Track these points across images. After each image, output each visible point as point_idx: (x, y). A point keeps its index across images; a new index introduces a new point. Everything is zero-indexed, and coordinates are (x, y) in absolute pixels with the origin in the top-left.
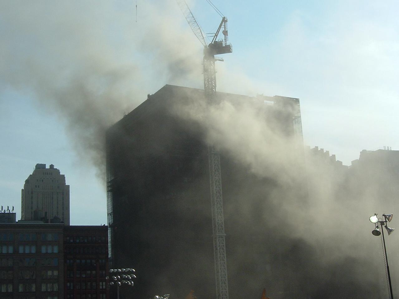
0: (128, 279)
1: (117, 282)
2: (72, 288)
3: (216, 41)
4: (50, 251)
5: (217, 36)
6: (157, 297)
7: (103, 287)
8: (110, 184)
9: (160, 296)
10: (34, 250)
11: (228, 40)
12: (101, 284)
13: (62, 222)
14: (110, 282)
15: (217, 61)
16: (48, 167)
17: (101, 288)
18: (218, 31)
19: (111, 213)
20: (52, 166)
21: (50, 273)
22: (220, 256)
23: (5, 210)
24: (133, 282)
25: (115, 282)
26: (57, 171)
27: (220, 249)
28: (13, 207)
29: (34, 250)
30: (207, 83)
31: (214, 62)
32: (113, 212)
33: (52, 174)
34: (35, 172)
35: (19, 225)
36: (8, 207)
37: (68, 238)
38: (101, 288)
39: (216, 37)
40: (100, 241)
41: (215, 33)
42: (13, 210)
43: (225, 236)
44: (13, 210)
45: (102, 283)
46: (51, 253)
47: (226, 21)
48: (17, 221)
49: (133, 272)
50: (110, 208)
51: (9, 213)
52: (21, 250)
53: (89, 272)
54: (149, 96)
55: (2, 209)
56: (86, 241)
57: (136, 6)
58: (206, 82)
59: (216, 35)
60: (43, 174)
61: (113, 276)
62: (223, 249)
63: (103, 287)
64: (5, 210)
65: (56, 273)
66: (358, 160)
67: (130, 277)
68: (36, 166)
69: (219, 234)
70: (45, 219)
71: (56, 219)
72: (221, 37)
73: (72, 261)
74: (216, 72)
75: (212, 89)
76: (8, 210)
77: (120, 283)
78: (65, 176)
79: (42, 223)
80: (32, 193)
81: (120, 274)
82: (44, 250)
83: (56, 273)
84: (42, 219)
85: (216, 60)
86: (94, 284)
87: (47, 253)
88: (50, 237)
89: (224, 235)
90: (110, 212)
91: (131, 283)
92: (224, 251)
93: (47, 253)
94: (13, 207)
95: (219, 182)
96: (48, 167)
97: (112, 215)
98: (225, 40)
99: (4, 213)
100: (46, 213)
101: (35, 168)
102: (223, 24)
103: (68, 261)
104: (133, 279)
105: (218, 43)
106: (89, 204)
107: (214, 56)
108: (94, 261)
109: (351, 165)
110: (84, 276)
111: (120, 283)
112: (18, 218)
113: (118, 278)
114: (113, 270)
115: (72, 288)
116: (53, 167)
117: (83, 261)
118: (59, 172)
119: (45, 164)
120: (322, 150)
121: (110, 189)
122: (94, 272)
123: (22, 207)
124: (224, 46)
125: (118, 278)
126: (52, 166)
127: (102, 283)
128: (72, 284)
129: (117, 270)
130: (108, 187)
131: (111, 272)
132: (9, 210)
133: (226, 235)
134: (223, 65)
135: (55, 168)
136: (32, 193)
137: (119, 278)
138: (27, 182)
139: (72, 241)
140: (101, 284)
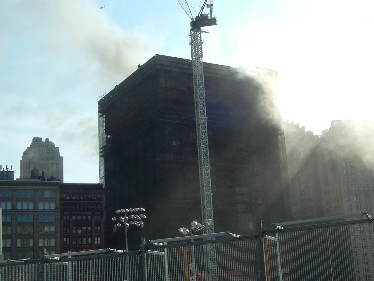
2: (68, 243)
3: (202, 14)
5: (203, 10)
6: (196, 222)
7: (98, 239)
8: (102, 150)
10: (31, 207)
11: (213, 13)
13: (59, 180)
15: (203, 33)
16: (43, 140)
17: (96, 243)
18: (204, 5)
19: (103, 176)
20: (47, 140)
21: (46, 229)
22: (207, 214)
23: (3, 169)
24: (143, 223)
25: (122, 223)
26: (53, 144)
27: (207, 207)
28: (12, 166)
29: (31, 207)
30: (194, 53)
31: (200, 34)
32: (104, 176)
33: (47, 147)
34: (32, 145)
35: (18, 183)
36: (7, 166)
37: (65, 195)
38: (96, 243)
39: (202, 10)
40: (95, 198)
41: (202, 7)
42: (12, 169)
43: (212, 195)
44: (12, 169)
46: (48, 210)
48: (15, 179)
49: (143, 212)
51: (8, 172)
52: (19, 207)
53: (84, 228)
54: (139, 66)
55: (1, 169)
58: (193, 52)
59: (202, 9)
60: (40, 146)
61: (120, 217)
62: (210, 208)
63: (98, 239)
65: (53, 229)
67: (139, 217)
69: (207, 193)
70: (42, 178)
72: (206, 11)
73: (68, 217)
74: (203, 43)
76: (6, 169)
77: (128, 224)
78: (59, 149)
84: (39, 178)
85: (202, 32)
86: (90, 240)
88: (47, 195)
89: (210, 195)
91: (141, 224)
92: (211, 210)
94: (12, 166)
96: (43, 140)
97: (104, 179)
98: (211, 12)
99: (3, 171)
101: (32, 141)
103: (65, 217)
104: (143, 219)
105: (204, 16)
106: (83, 167)
107: (200, 28)
108: (89, 217)
109: (321, 134)
110: (80, 231)
111: (128, 224)
112: (17, 176)
115: (68, 243)
116: (49, 140)
117: (79, 217)
121: (102, 154)
122: (89, 228)
123: (20, 167)
124: (210, 18)
126: (47, 140)
128: (68, 239)
129: (125, 210)
132: (8, 169)
133: (213, 194)
134: (208, 34)
135: (50, 141)
136: (29, 164)
139: (68, 198)
140: (97, 240)
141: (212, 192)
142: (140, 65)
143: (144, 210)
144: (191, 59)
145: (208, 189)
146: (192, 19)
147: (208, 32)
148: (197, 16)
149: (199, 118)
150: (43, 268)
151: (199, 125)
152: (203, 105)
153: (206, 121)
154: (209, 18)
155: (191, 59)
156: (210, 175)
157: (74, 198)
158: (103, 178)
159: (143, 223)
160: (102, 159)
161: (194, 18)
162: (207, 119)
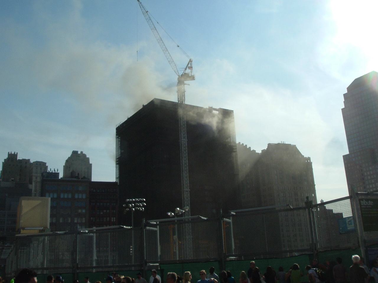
0: (140, 206)
1: (131, 209)
2: (94, 221)
4: (80, 197)
8: (117, 160)
9: (180, 208)
10: (70, 196)
12: (112, 218)
14: (126, 209)
20: (82, 152)
21: (80, 211)
23: (52, 171)
25: (130, 208)
28: (58, 170)
29: (70, 196)
31: (184, 86)
35: (62, 180)
36: (54, 169)
42: (58, 171)
44: (58, 171)
45: (113, 221)
47: (192, 61)
50: (118, 174)
51: (55, 173)
53: (105, 211)
56: (103, 191)
57: (136, 52)
64: (52, 171)
65: (84, 211)
66: (265, 149)
68: (72, 152)
71: (84, 177)
74: (185, 91)
75: (182, 102)
79: (75, 179)
80: (69, 168)
81: (134, 202)
82: (76, 196)
83: (84, 211)
84: (76, 177)
85: (185, 84)
86: (108, 219)
87: (78, 198)
90: (117, 177)
93: (78, 198)
94: (58, 170)
95: (186, 158)
96: (79, 153)
99: (52, 172)
100: (78, 174)
102: (190, 63)
104: (144, 206)
111: (134, 209)
112: (61, 176)
113: (132, 205)
114: (128, 200)
115: (94, 221)
118: (86, 156)
119: (78, 151)
120: (243, 144)
121: (118, 163)
122: (108, 211)
125: (132, 205)
126: (82, 152)
127: (113, 221)
130: (117, 161)
131: (127, 201)
137: (133, 206)
138: (67, 161)
139: (94, 191)
141: (190, 189)
142: (144, 105)
143: (145, 200)
144: (178, 102)
145: (185, 163)
146: (179, 76)
147: (189, 85)
148: (182, 74)
149: (182, 141)
150: (76, 237)
151: (182, 145)
152: (185, 145)
153: (186, 142)
154: (190, 75)
155: (178, 102)
156: (188, 178)
157: (98, 191)
158: (118, 178)
159: (143, 209)
160: (118, 166)
161: (180, 75)
162: (190, 191)
